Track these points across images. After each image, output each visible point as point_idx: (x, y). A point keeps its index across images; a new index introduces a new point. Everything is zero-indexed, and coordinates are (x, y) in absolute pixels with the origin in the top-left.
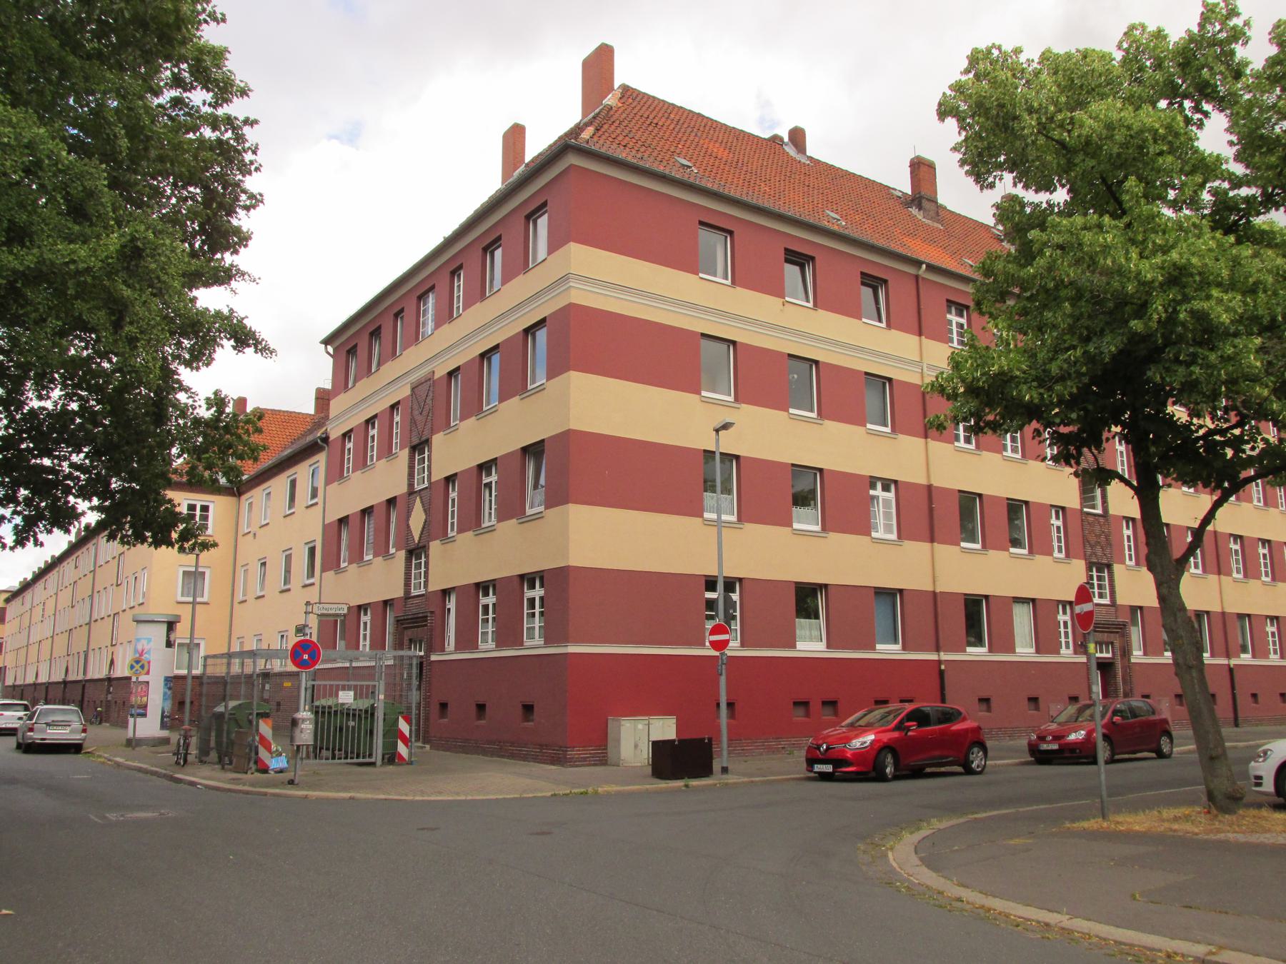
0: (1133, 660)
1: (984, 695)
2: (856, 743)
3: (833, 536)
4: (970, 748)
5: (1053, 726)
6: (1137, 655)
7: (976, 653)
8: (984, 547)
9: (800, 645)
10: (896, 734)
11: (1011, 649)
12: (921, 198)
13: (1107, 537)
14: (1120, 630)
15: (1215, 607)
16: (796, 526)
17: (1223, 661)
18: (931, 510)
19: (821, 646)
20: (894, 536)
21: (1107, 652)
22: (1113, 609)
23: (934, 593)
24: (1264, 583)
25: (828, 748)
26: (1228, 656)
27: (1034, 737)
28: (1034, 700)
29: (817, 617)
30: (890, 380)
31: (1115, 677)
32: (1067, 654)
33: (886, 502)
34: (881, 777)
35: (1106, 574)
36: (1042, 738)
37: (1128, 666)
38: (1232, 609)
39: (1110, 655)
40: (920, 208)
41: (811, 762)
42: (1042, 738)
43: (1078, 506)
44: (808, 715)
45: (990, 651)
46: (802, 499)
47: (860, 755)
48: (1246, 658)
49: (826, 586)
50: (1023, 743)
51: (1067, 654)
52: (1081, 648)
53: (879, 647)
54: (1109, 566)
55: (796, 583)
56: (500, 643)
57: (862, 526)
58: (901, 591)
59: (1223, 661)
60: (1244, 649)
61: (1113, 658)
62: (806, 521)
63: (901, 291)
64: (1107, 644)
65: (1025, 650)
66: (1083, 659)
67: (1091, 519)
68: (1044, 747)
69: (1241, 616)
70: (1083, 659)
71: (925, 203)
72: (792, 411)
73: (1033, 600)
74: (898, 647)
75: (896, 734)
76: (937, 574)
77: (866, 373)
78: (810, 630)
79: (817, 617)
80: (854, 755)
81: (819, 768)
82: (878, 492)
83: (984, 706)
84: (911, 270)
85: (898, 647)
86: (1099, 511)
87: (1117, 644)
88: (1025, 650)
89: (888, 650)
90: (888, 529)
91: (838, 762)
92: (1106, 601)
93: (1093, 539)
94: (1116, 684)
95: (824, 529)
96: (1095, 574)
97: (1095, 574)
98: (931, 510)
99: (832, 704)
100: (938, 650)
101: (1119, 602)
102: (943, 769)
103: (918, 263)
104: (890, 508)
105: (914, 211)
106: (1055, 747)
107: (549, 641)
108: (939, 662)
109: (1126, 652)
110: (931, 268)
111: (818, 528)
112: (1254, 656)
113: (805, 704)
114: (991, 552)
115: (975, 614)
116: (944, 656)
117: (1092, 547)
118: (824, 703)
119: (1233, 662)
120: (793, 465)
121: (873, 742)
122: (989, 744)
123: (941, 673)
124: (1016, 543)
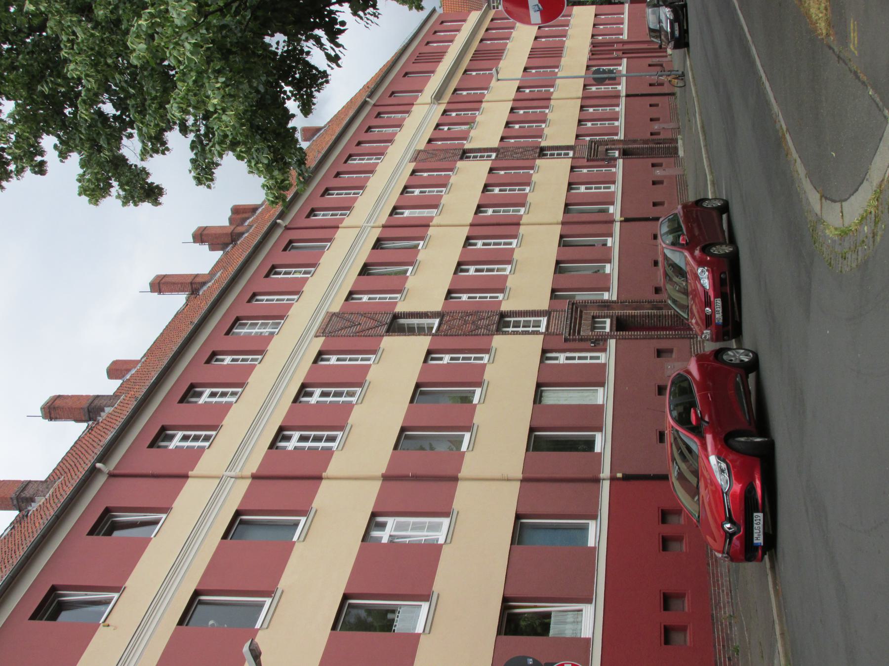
0: (615, 298)
2: (722, 480)
3: (439, 585)
4: (724, 362)
7: (602, 443)
8: (468, 428)
9: (586, 633)
10: (709, 438)
11: (599, 409)
12: (18, 498)
13: (468, 314)
14: (577, 310)
15: (557, 230)
16: (419, 629)
17: (617, 227)
18: (416, 478)
19: (588, 610)
20: (445, 521)
21: (605, 322)
22: (554, 314)
23: (524, 480)
25: (730, 520)
26: (612, 222)
27: (707, 333)
29: (548, 615)
30: (238, 513)
31: (634, 317)
32: (607, 357)
33: (398, 527)
34: (770, 447)
35: (512, 319)
37: (620, 303)
39: (608, 321)
40: (31, 500)
41: (749, 552)
43: (429, 338)
44: (683, 629)
45: (600, 429)
46: (383, 621)
47: (737, 472)
49: (505, 600)
51: (607, 357)
52: (599, 344)
53: (591, 543)
54: (503, 315)
55: (499, 633)
57: (430, 553)
58: (518, 517)
61: (611, 318)
62: (414, 618)
63: (124, 494)
64: (594, 322)
66: (612, 343)
67: (445, 327)
68: (719, 317)
69: (567, 210)
71: (27, 494)
72: (258, 626)
73: (539, 385)
74: (592, 525)
75: (709, 438)
76: (498, 475)
77: (225, 537)
78: (565, 623)
79: (548, 615)
80: (738, 480)
81: (758, 538)
82: (384, 536)
84: (101, 481)
85: (592, 525)
86: (436, 322)
87: (596, 312)
89: (596, 534)
90: (437, 527)
91: (749, 504)
92: (544, 321)
93: (470, 327)
94: (642, 316)
95: (426, 597)
96: (510, 329)
97: (510, 329)
98: (416, 478)
99: (664, 516)
100: (597, 480)
101: (546, 308)
103: (93, 472)
104: (408, 524)
105: (33, 507)
106: (718, 302)
108: (613, 479)
110: (104, 457)
111: (425, 606)
113: (668, 633)
114: (476, 421)
115: (553, 442)
116: (606, 472)
117: (478, 328)
118: (667, 641)
120: (334, 628)
121: (719, 457)
123: (627, 478)
124: (466, 399)
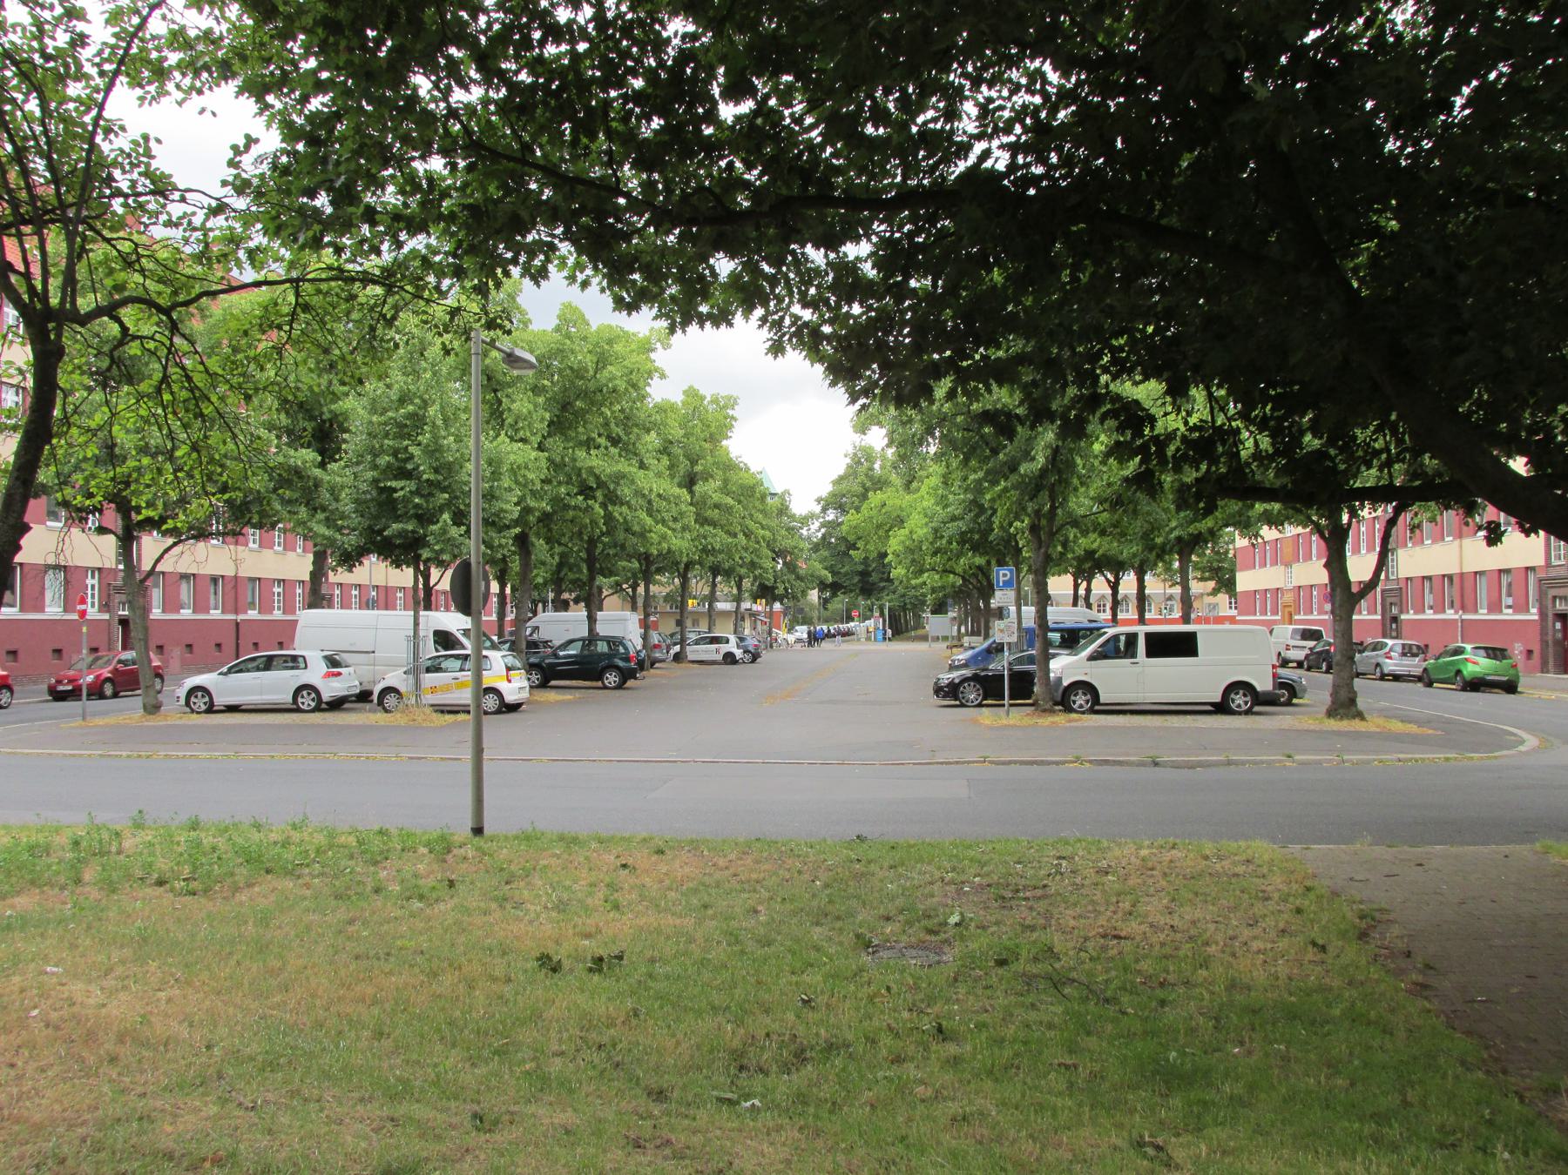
1: (12, 648)
5: (71, 673)
6: (156, 613)
15: (1453, 569)
17: (232, 617)
24: (277, 553)
28: (58, 652)
32: (93, 613)
36: (59, 682)
38: (1469, 568)
42: (59, 682)
48: (253, 614)
50: (45, 687)
52: (105, 606)
56: (1490, 611)
59: (232, 617)
60: (252, 605)
65: (53, 610)
68: (61, 688)
70: (106, 616)
83: (11, 657)
88: (53, 610)
102: (1413, 728)
107: (1490, 611)
109: (146, 610)
112: (22, 610)
119: (241, 617)
122: (15, 688)
